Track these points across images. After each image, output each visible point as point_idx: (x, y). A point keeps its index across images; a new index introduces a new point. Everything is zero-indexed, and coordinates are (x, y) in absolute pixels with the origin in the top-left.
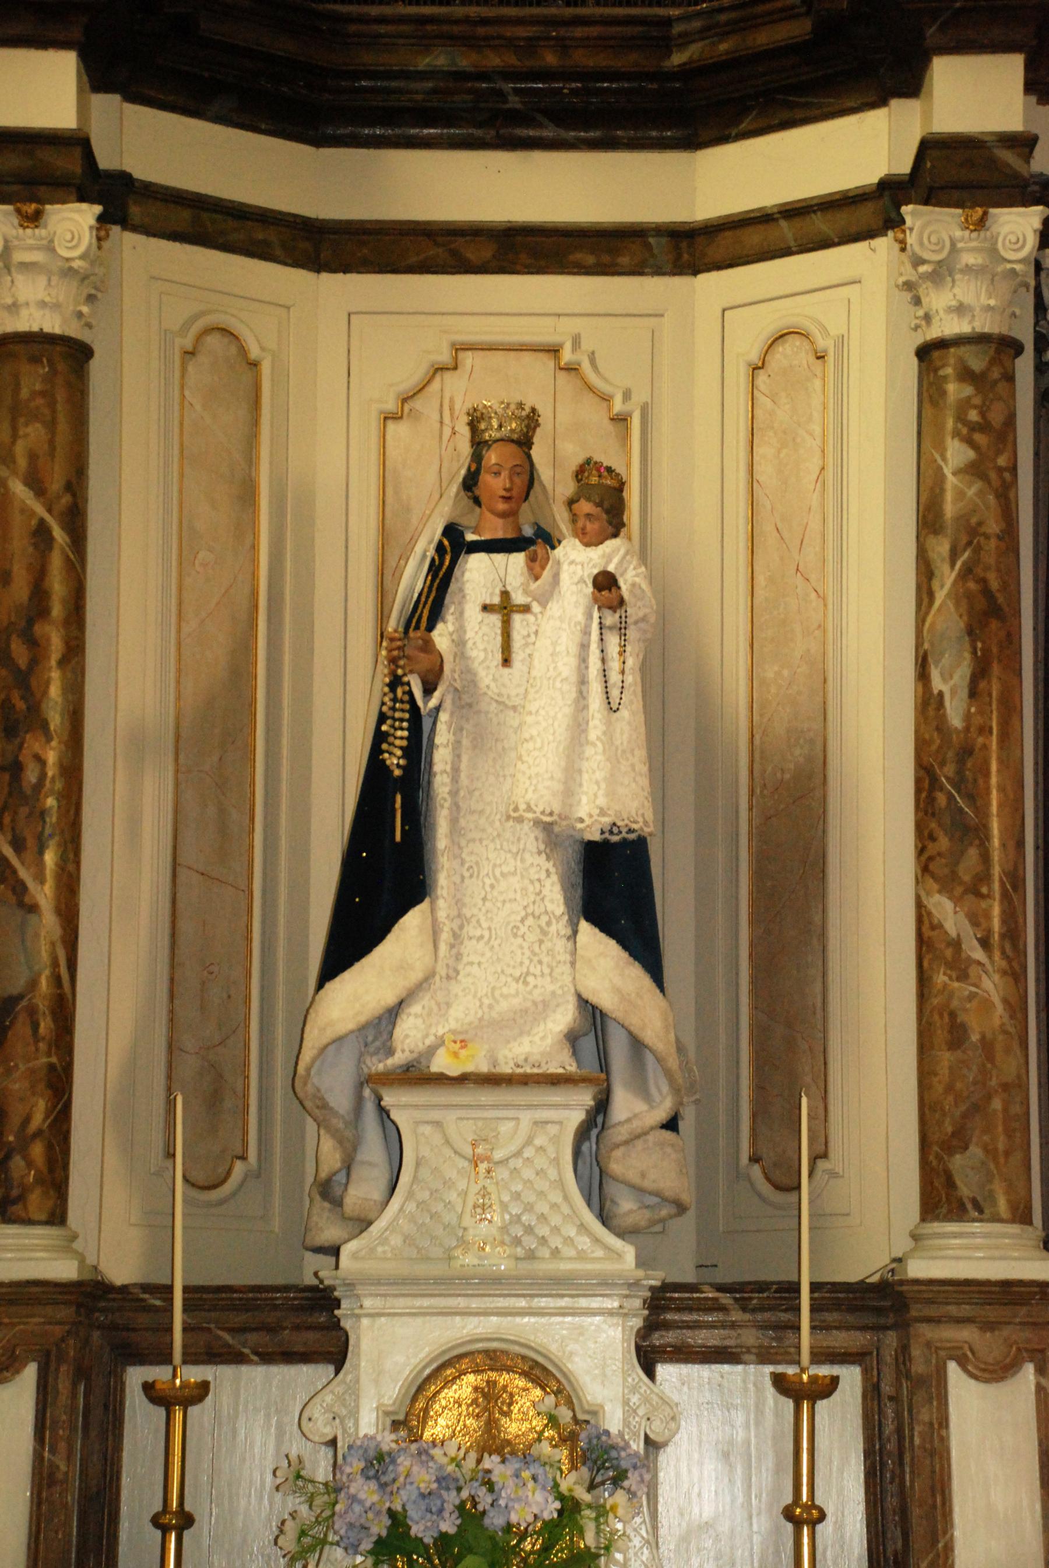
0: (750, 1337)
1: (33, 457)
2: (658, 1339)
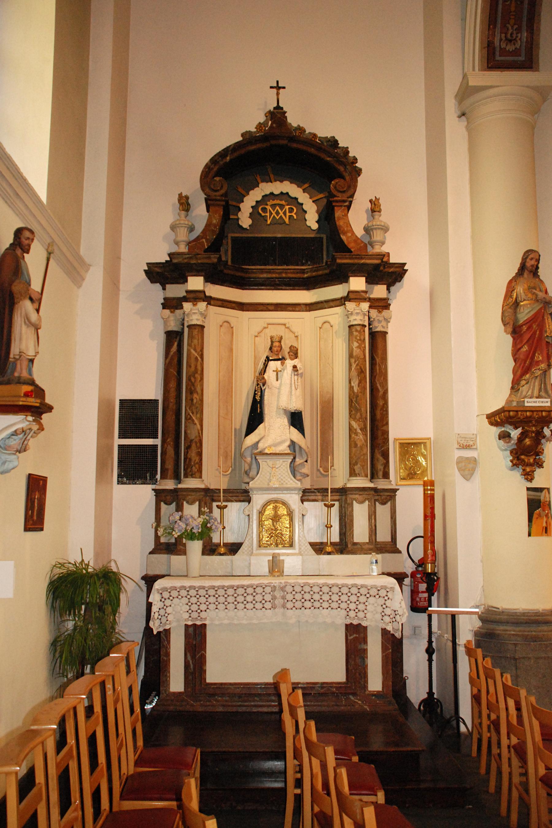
0: (320, 497)
1: (195, 346)
2: (304, 498)
